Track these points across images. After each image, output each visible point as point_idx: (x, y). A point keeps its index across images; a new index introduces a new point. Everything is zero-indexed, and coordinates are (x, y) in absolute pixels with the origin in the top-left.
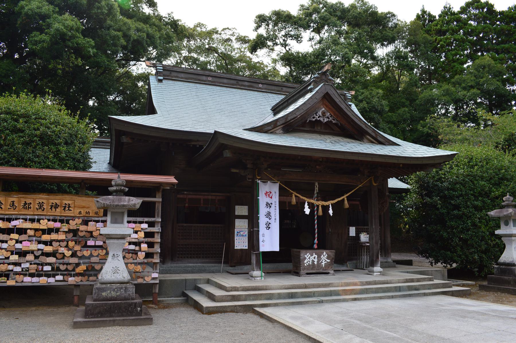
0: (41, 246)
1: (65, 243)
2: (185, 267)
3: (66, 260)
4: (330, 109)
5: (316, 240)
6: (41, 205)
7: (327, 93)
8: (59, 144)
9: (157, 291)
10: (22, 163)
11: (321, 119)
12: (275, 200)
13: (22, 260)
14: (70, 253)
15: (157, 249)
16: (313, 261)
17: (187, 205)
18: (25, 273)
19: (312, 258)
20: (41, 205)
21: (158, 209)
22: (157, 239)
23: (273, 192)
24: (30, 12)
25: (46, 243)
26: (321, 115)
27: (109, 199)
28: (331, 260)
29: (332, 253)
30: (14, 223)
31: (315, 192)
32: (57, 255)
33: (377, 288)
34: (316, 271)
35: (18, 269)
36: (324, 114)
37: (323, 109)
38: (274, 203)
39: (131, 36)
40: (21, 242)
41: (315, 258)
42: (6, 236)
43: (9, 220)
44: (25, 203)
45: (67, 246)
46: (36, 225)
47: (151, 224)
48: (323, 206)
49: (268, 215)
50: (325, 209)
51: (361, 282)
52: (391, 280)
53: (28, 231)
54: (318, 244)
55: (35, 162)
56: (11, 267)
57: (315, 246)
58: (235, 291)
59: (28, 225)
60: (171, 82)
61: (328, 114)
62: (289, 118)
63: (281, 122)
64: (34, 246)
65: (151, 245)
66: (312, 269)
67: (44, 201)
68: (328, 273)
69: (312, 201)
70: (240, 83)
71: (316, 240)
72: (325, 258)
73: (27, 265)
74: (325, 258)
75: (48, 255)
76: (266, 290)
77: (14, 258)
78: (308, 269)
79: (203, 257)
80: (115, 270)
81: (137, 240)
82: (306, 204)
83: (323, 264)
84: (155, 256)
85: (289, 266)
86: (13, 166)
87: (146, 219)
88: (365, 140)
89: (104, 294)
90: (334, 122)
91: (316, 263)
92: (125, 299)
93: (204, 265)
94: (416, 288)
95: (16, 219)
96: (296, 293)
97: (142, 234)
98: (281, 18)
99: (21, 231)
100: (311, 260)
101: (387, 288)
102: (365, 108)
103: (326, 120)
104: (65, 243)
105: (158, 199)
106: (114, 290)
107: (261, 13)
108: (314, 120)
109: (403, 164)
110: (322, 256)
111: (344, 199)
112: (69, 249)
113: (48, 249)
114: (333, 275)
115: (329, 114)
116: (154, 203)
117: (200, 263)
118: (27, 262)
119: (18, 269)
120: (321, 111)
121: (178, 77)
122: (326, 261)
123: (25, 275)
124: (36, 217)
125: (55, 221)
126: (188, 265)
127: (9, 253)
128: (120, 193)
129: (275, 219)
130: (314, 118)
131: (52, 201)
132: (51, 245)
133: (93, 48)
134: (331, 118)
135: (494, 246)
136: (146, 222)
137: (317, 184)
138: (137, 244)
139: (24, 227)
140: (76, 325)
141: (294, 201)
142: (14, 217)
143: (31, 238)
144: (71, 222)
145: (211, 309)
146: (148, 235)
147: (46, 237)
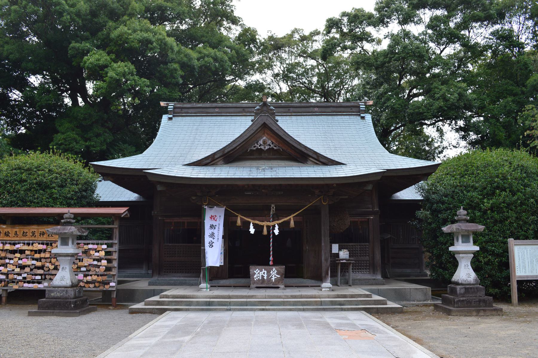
0: (34, 262)
1: (50, 260)
2: (170, 280)
3: (50, 272)
4: (271, 136)
5: (271, 257)
6: (33, 233)
7: (264, 123)
8: (54, 188)
9: (115, 296)
10: (25, 203)
11: (262, 147)
12: (220, 223)
13: (22, 271)
14: (53, 266)
15: (115, 264)
16: (263, 276)
17: (172, 228)
18: (24, 280)
19: (261, 273)
20: (33, 233)
21: (116, 233)
22: (115, 256)
23: (218, 216)
24: (90, 66)
25: (37, 260)
26: (262, 143)
27: (57, 229)
28: (281, 276)
29: (282, 268)
30: (18, 246)
31: (271, 213)
32: (45, 268)
33: (295, 301)
34: (265, 285)
35: (20, 278)
36: (265, 142)
37: (264, 138)
38: (217, 225)
39: (194, 66)
40: (21, 259)
41: (264, 273)
42: (12, 255)
43: (14, 244)
44: (24, 233)
45: (50, 262)
46: (30, 248)
47: (109, 246)
48: (268, 227)
49: (212, 235)
50: (270, 229)
51: (285, 295)
52: (319, 295)
53: (26, 251)
54: (273, 261)
55: (34, 202)
56: (15, 276)
57: (271, 263)
58: (166, 298)
59: (25, 247)
60: (180, 118)
61: (269, 142)
62: (226, 151)
63: (221, 154)
64: (30, 262)
65: (109, 261)
66: (262, 283)
67: (35, 230)
68: (278, 288)
69: (257, 222)
70: (246, 110)
71: (271, 257)
72: (275, 274)
73: (25, 275)
74: (275, 274)
75: (39, 268)
76: (193, 298)
77: (18, 270)
78: (257, 284)
79: (186, 272)
80: (64, 277)
81: (99, 258)
82: (251, 225)
83: (273, 279)
84: (113, 270)
85: (242, 281)
86: (20, 206)
87: (106, 242)
88: (309, 162)
89: (52, 294)
90: (275, 148)
91: (265, 278)
92: (66, 298)
93: (186, 278)
94: (340, 304)
95: (19, 243)
96: (213, 301)
97: (102, 254)
98: (357, 18)
99: (22, 252)
100: (260, 275)
101: (306, 301)
102: (441, 107)
103: (267, 147)
104: (49, 260)
105: (115, 226)
106: (59, 292)
107: (331, 16)
108: (255, 149)
109: (337, 184)
110: (272, 272)
111: (290, 219)
112: (52, 265)
113: (39, 264)
114: (284, 289)
115: (270, 141)
116: (111, 229)
117: (183, 277)
118: (25, 273)
119: (20, 278)
120: (262, 140)
121: (188, 113)
122: (275, 276)
123: (25, 282)
124: (31, 242)
125: (43, 244)
126: (172, 278)
127: (15, 267)
128: (69, 223)
129: (218, 239)
130: (255, 147)
131: (40, 230)
132: (40, 261)
133: (148, 86)
134: (272, 145)
135: (487, 263)
136: (106, 244)
137: (273, 205)
138: (99, 260)
139: (23, 249)
140: (31, 314)
141: (239, 222)
142: (17, 242)
143: (28, 257)
144: (53, 244)
145: (134, 310)
146: (108, 253)
147: (37, 256)
